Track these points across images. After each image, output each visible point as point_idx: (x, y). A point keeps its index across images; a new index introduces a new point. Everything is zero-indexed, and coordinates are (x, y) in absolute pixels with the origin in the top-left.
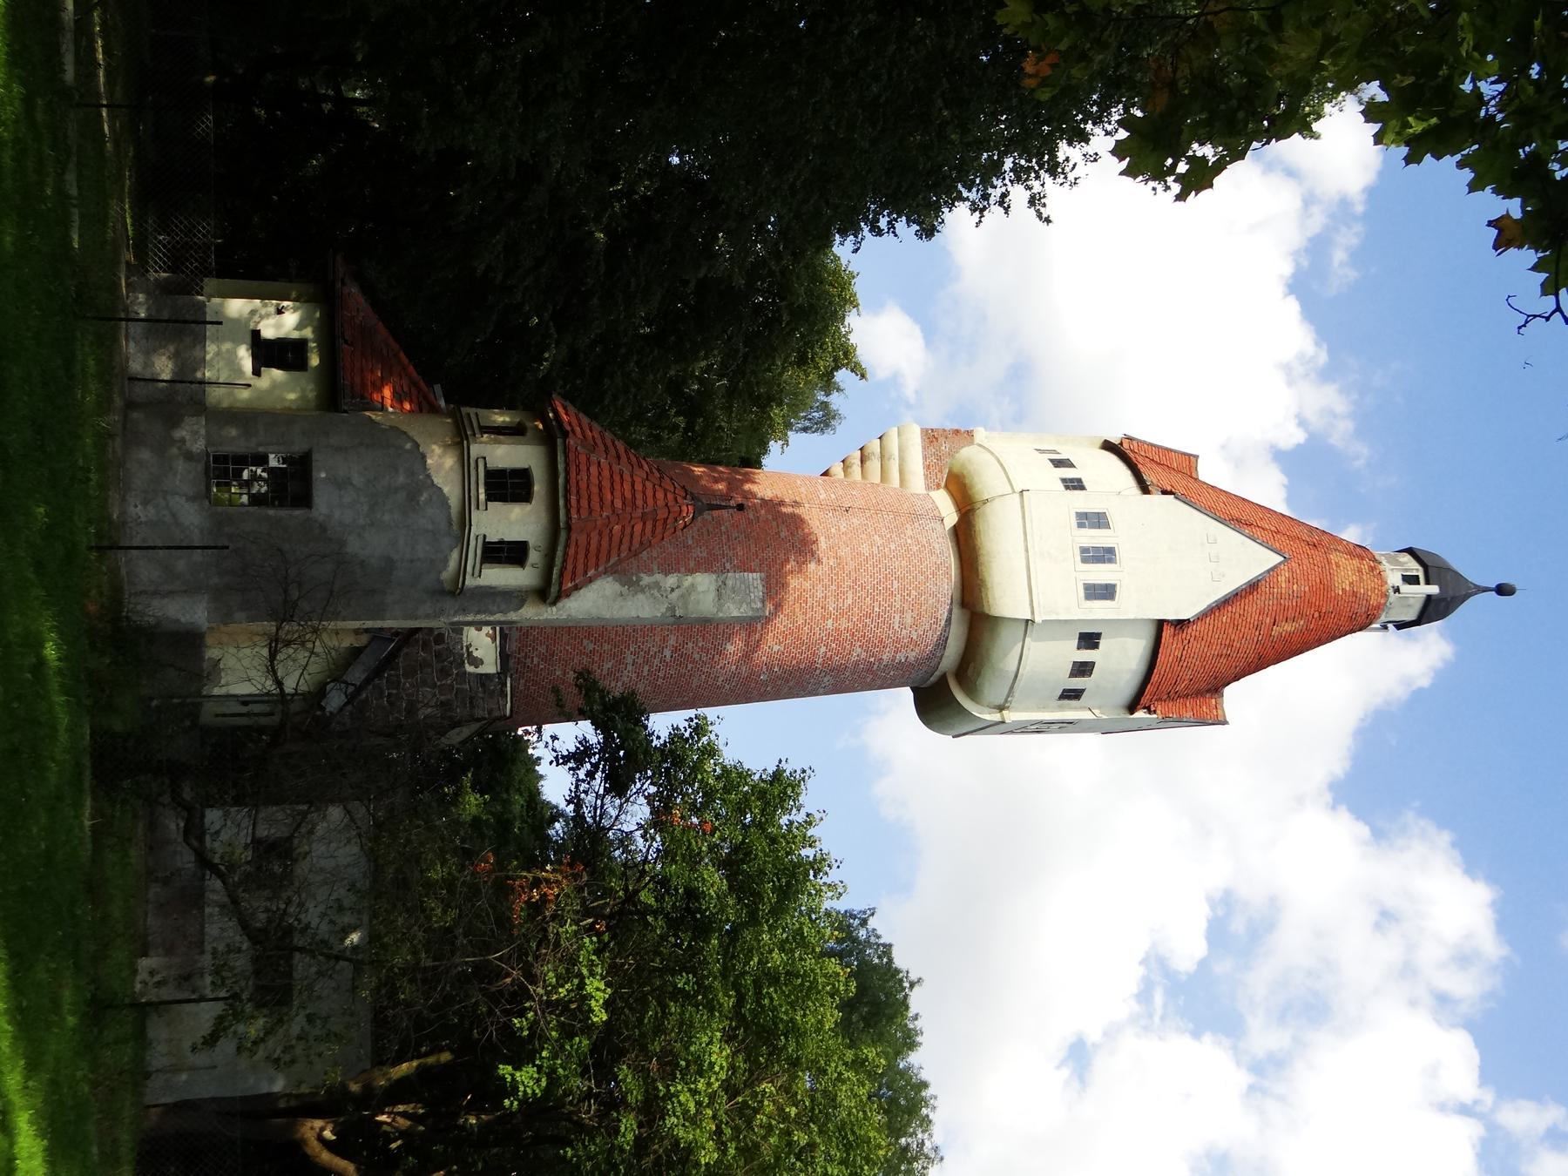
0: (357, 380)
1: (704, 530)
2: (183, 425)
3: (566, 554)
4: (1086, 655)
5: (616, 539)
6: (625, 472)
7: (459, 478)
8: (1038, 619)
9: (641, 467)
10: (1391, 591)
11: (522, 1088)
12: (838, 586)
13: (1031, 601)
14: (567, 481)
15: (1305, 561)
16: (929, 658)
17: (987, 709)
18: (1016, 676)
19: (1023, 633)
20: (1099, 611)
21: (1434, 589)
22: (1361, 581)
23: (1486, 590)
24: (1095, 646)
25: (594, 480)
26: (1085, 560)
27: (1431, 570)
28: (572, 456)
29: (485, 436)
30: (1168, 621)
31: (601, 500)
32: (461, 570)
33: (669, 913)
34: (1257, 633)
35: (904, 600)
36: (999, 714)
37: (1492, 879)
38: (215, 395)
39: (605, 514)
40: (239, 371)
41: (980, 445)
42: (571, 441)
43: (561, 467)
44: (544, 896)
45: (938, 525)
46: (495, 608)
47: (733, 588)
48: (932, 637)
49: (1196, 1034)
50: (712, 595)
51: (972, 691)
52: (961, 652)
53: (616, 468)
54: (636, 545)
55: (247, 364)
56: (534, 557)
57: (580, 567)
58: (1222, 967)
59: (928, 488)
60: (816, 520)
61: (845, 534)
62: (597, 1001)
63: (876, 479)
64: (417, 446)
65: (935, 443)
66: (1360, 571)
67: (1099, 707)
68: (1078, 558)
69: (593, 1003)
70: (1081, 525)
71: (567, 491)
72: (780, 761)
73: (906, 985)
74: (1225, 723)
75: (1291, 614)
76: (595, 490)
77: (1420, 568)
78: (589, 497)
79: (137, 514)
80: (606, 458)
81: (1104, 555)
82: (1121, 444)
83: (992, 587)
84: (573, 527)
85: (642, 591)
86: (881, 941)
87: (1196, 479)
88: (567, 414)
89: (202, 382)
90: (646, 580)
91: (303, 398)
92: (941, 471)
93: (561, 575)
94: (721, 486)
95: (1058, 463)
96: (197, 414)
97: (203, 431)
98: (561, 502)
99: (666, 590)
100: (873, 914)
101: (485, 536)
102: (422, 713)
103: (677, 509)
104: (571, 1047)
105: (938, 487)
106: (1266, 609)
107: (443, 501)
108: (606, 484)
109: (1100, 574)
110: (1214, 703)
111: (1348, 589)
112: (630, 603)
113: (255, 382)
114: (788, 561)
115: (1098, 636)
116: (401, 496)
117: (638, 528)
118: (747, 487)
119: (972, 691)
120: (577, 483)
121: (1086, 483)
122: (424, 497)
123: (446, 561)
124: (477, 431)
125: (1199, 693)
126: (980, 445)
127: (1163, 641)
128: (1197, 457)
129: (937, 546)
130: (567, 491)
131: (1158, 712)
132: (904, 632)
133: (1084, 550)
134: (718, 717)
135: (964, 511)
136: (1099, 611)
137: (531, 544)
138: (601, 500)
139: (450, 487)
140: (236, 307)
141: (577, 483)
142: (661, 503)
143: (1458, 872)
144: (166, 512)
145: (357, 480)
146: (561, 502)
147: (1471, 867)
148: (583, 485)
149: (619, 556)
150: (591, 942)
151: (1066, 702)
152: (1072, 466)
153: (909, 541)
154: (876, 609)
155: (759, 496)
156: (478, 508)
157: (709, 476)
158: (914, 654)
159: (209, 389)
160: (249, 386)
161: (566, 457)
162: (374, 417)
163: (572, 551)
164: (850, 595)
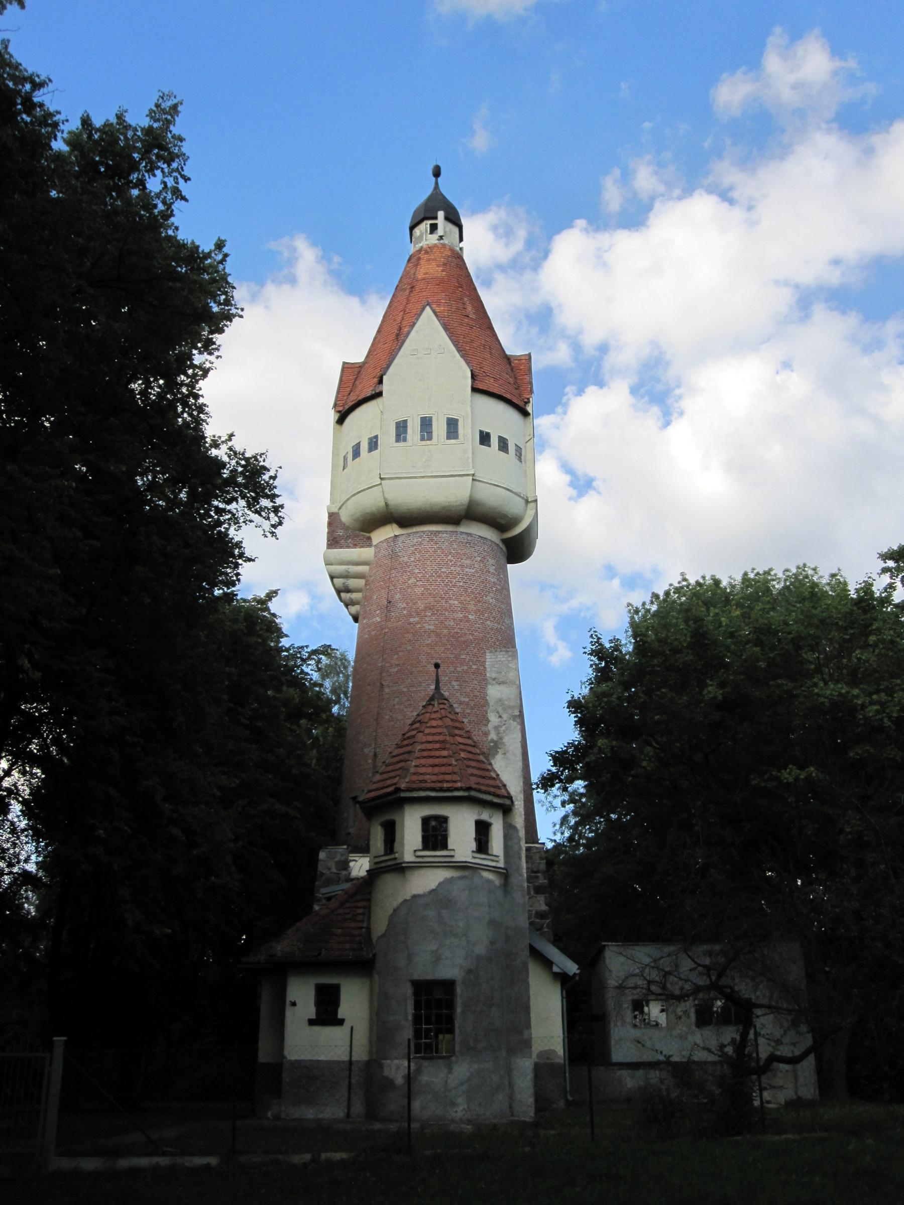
1: (406, 704)
2: (391, 1077)
3: (485, 792)
5: (470, 756)
6: (419, 747)
9: (413, 737)
10: (442, 241)
12: (446, 610)
18: (508, 490)
19: (480, 483)
21: (441, 214)
22: (435, 260)
23: (437, 184)
25: (430, 770)
26: (430, 438)
27: (428, 215)
32: (494, 870)
34: (474, 328)
35: (455, 565)
38: (361, 1054)
39: (454, 763)
42: (403, 786)
43: (422, 794)
45: (400, 539)
47: (498, 673)
50: (502, 688)
53: (417, 754)
56: (485, 816)
59: (370, 545)
61: (407, 604)
63: (361, 583)
65: (338, 539)
66: (429, 260)
68: (428, 442)
70: (405, 440)
71: (441, 790)
72: (585, 653)
75: (461, 306)
76: (437, 770)
77: (426, 222)
78: (442, 774)
79: (462, 1111)
80: (412, 761)
81: (426, 424)
82: (339, 412)
83: (449, 502)
84: (468, 786)
85: (501, 738)
87: (364, 363)
90: (493, 736)
93: (498, 796)
95: (356, 453)
96: (381, 1066)
99: (501, 721)
101: (473, 852)
102: (544, 907)
103: (443, 711)
105: (369, 538)
106: (458, 321)
107: (448, 882)
109: (439, 428)
110: (516, 361)
111: (442, 268)
112: (511, 748)
115: (481, 432)
116: (445, 913)
117: (459, 739)
120: (433, 782)
124: (392, 856)
126: (340, 508)
127: (485, 389)
128: (344, 363)
129: (416, 540)
130: (441, 790)
131: (528, 397)
132: (476, 566)
134: (568, 693)
141: (433, 782)
142: (440, 723)
148: (434, 778)
149: (479, 754)
151: (523, 458)
153: (412, 559)
154: (461, 584)
156: (453, 856)
163: (483, 788)
164: (451, 602)
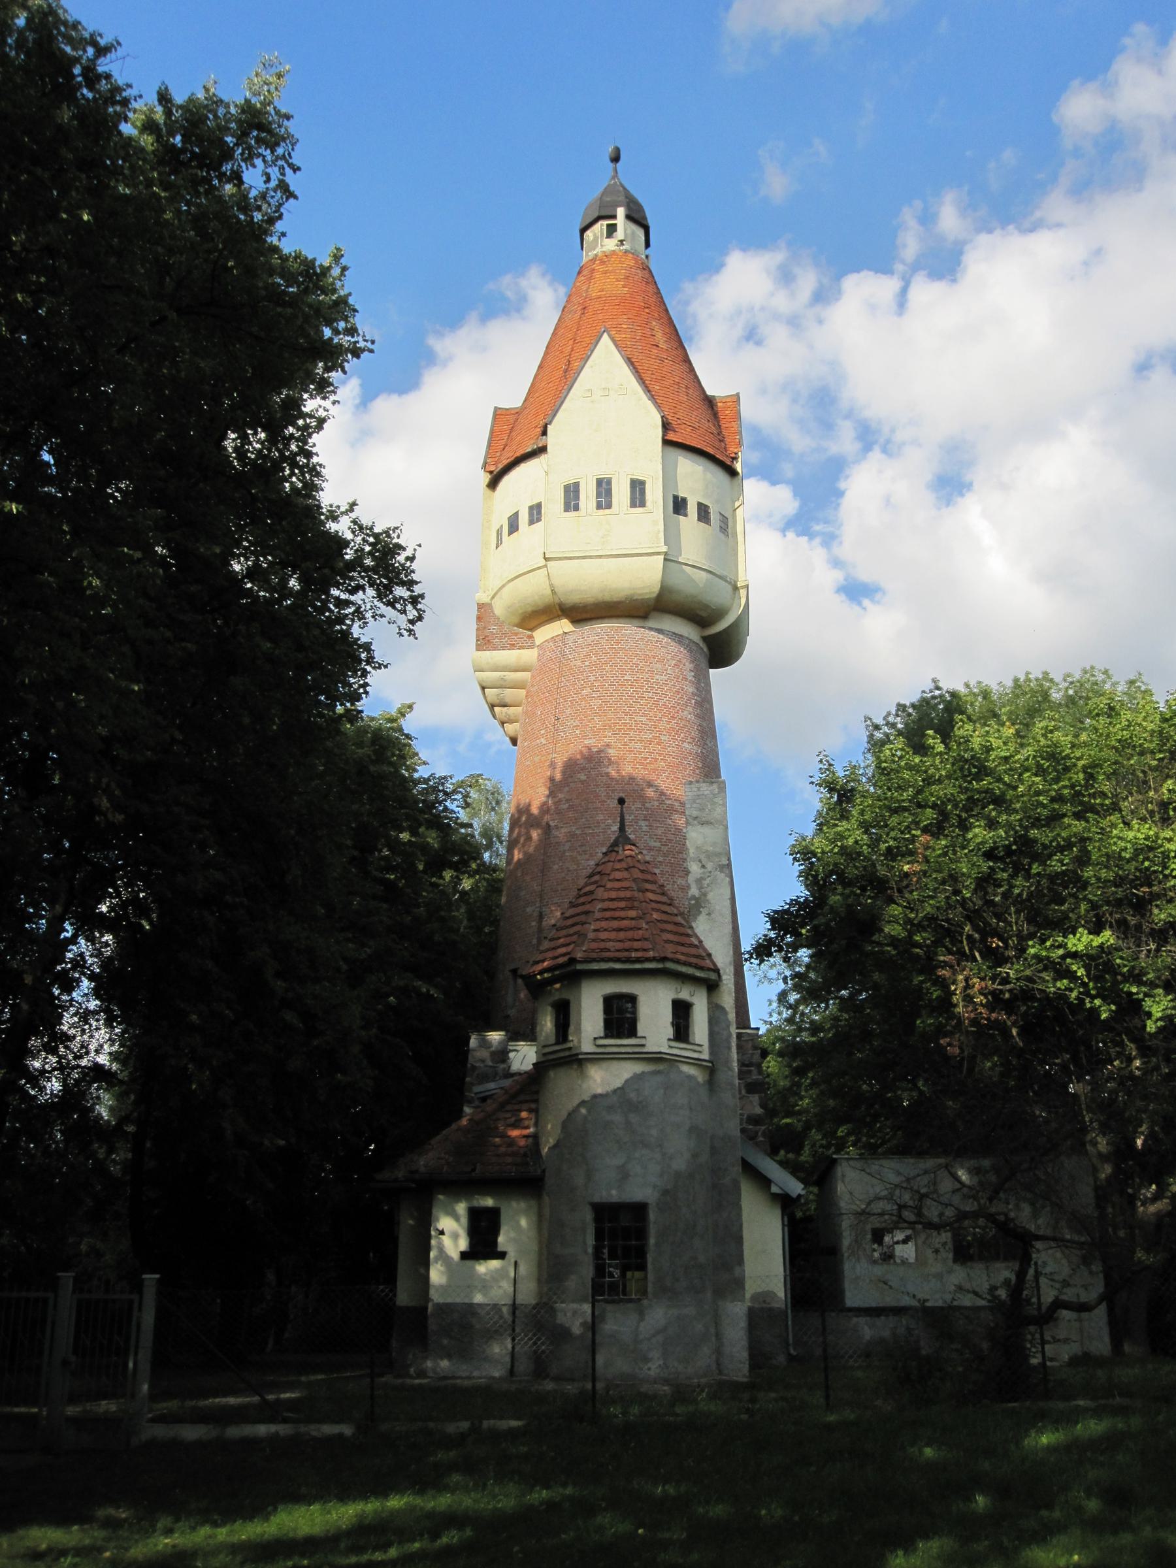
0: (509, 1160)
2: (567, 1325)
3: (685, 964)
4: (692, 509)
5: (664, 917)
7: (615, 1063)
8: (664, 549)
9: (592, 892)
11: (1169, 1012)
14: (618, 960)
15: (600, 316)
16: (690, 651)
17: (736, 600)
20: (655, 494)
24: (684, 500)
25: (613, 935)
27: (603, 213)
29: (571, 1038)
30: (664, 435)
31: (631, 929)
32: (697, 1063)
33: (1009, 875)
36: (741, 591)
37: (724, 252)
38: (528, 1294)
39: (644, 925)
40: (500, 1274)
41: (493, 597)
44: (981, 992)
45: (570, 639)
46: (725, 1033)
47: (700, 810)
48: (674, 647)
49: (840, 494)
50: (706, 830)
51: (719, 614)
52: (686, 622)
53: (598, 915)
54: (664, 899)
55: (495, 1264)
56: (684, 995)
58: (788, 470)
59: (532, 646)
62: (1092, 940)
67: (733, 502)
68: (607, 511)
69: (1095, 944)
70: (576, 508)
72: (812, 783)
73: (937, 693)
74: (738, 395)
76: (622, 935)
77: (600, 222)
78: (630, 940)
81: (604, 488)
82: (491, 472)
84: (663, 955)
85: (705, 895)
88: (543, 961)
90: (694, 891)
92: (516, 634)
93: (701, 968)
94: (535, 834)
95: (513, 526)
96: (552, 1311)
98: (638, 966)
99: (704, 873)
100: (870, 719)
101: (669, 1040)
104: (1125, 966)
105: (531, 637)
107: (637, 1078)
108: (615, 924)
109: (621, 493)
112: (717, 907)
114: (607, 774)
115: (675, 498)
116: (634, 1118)
118: (535, 810)
119: (719, 614)
120: (618, 951)
121: (535, 502)
122: (633, 1095)
123: (690, 1077)
125: (715, 415)
126: (493, 597)
129: (591, 639)
131: (736, 450)
135: (560, 613)
138: (631, 929)
140: (437, 1275)
141: (618, 951)
142: (625, 874)
143: (715, 278)
145: (619, 1160)
146: (638, 966)
147: (716, 267)
148: (619, 945)
152: (516, 514)
154: (650, 695)
157: (523, 846)
158: (687, 664)
159: (518, 1301)
160: (516, 1263)
161: (594, 960)
162: (552, 1141)
163: (682, 958)
164: (637, 718)
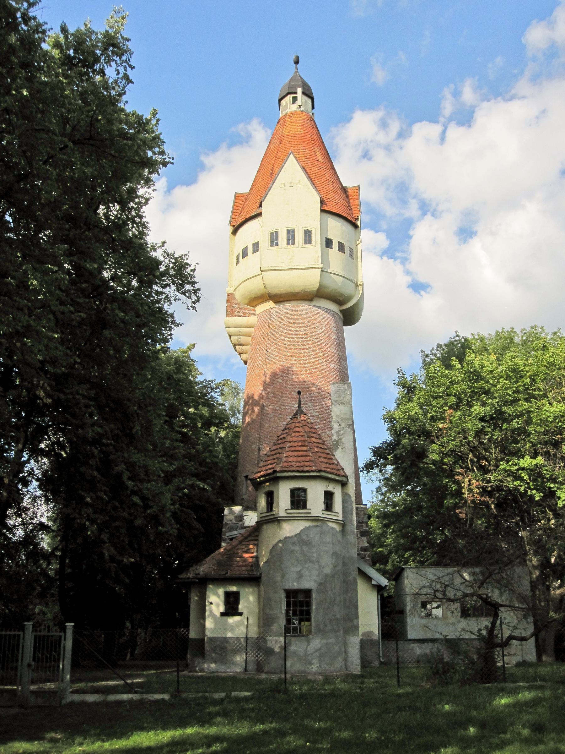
0: (244, 568)
3: (330, 473)
4: (335, 245)
5: (321, 450)
7: (296, 521)
8: (321, 265)
9: (284, 438)
13: (312, 268)
14: (298, 471)
15: (289, 145)
16: (334, 317)
17: (357, 292)
18: (344, 277)
20: (316, 237)
24: (331, 240)
25: (295, 459)
26: (293, 243)
28: (286, 469)
30: (321, 207)
32: (336, 521)
40: (241, 623)
41: (235, 290)
42: (278, 469)
45: (274, 311)
48: (326, 315)
49: (410, 237)
50: (341, 407)
51: (348, 299)
53: (287, 449)
54: (320, 441)
55: (237, 618)
56: (330, 488)
57: (334, 467)
59: (254, 315)
60: (274, 366)
61: (279, 353)
64: (280, 541)
67: (356, 241)
68: (292, 246)
70: (277, 245)
71: (302, 471)
72: (394, 384)
73: (457, 338)
74: (359, 186)
75: (313, 153)
76: (299, 459)
81: (291, 234)
82: (234, 226)
85: (341, 439)
86: (436, 348)
88: (260, 472)
89: (247, 639)
90: (335, 437)
91: (252, 594)
92: (247, 309)
93: (339, 475)
95: (245, 254)
96: (265, 641)
97: (276, 638)
98: (307, 474)
105: (254, 310)
107: (307, 529)
108: (296, 454)
109: (299, 237)
113: (245, 614)
115: (327, 239)
116: (305, 548)
117: (314, 440)
121: (256, 241)
126: (235, 290)
129: (284, 311)
130: (302, 471)
133: (288, 244)
136: (316, 237)
137: (326, 489)
139: (303, 525)
140: (209, 624)
142: (301, 429)
143: (347, 125)
144: (315, 655)
145: (298, 569)
146: (307, 474)
148: (298, 464)
150: (503, 465)
153: (282, 324)
155: (261, 392)
156: (310, 513)
157: (251, 415)
160: (247, 618)
161: (285, 471)
